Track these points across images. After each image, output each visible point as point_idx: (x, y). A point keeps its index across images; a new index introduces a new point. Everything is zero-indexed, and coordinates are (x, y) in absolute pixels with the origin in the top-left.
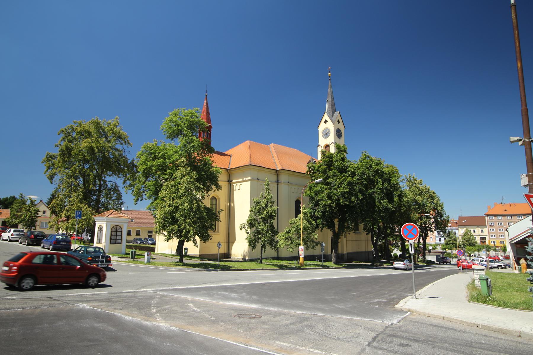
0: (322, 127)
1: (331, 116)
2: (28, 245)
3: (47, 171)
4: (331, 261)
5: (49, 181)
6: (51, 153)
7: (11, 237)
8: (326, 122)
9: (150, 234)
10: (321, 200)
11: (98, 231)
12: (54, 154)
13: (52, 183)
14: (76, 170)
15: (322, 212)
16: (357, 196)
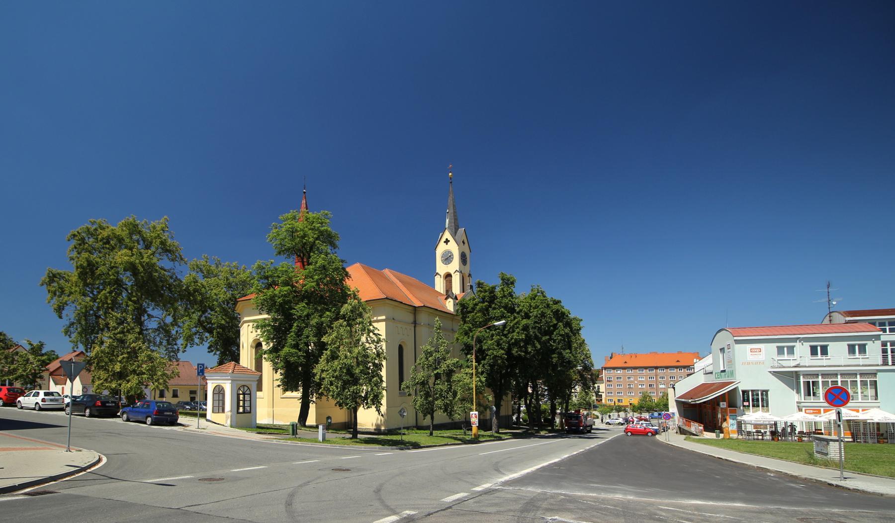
0: (441, 248)
1: (454, 235)
2: (91, 416)
3: (52, 299)
4: (491, 429)
5: (55, 315)
6: (54, 271)
7: (41, 403)
8: (447, 241)
9: (193, 396)
10: (489, 349)
11: (214, 394)
12: (59, 271)
13: (61, 317)
14: (106, 298)
15: (490, 365)
16: (534, 346)
